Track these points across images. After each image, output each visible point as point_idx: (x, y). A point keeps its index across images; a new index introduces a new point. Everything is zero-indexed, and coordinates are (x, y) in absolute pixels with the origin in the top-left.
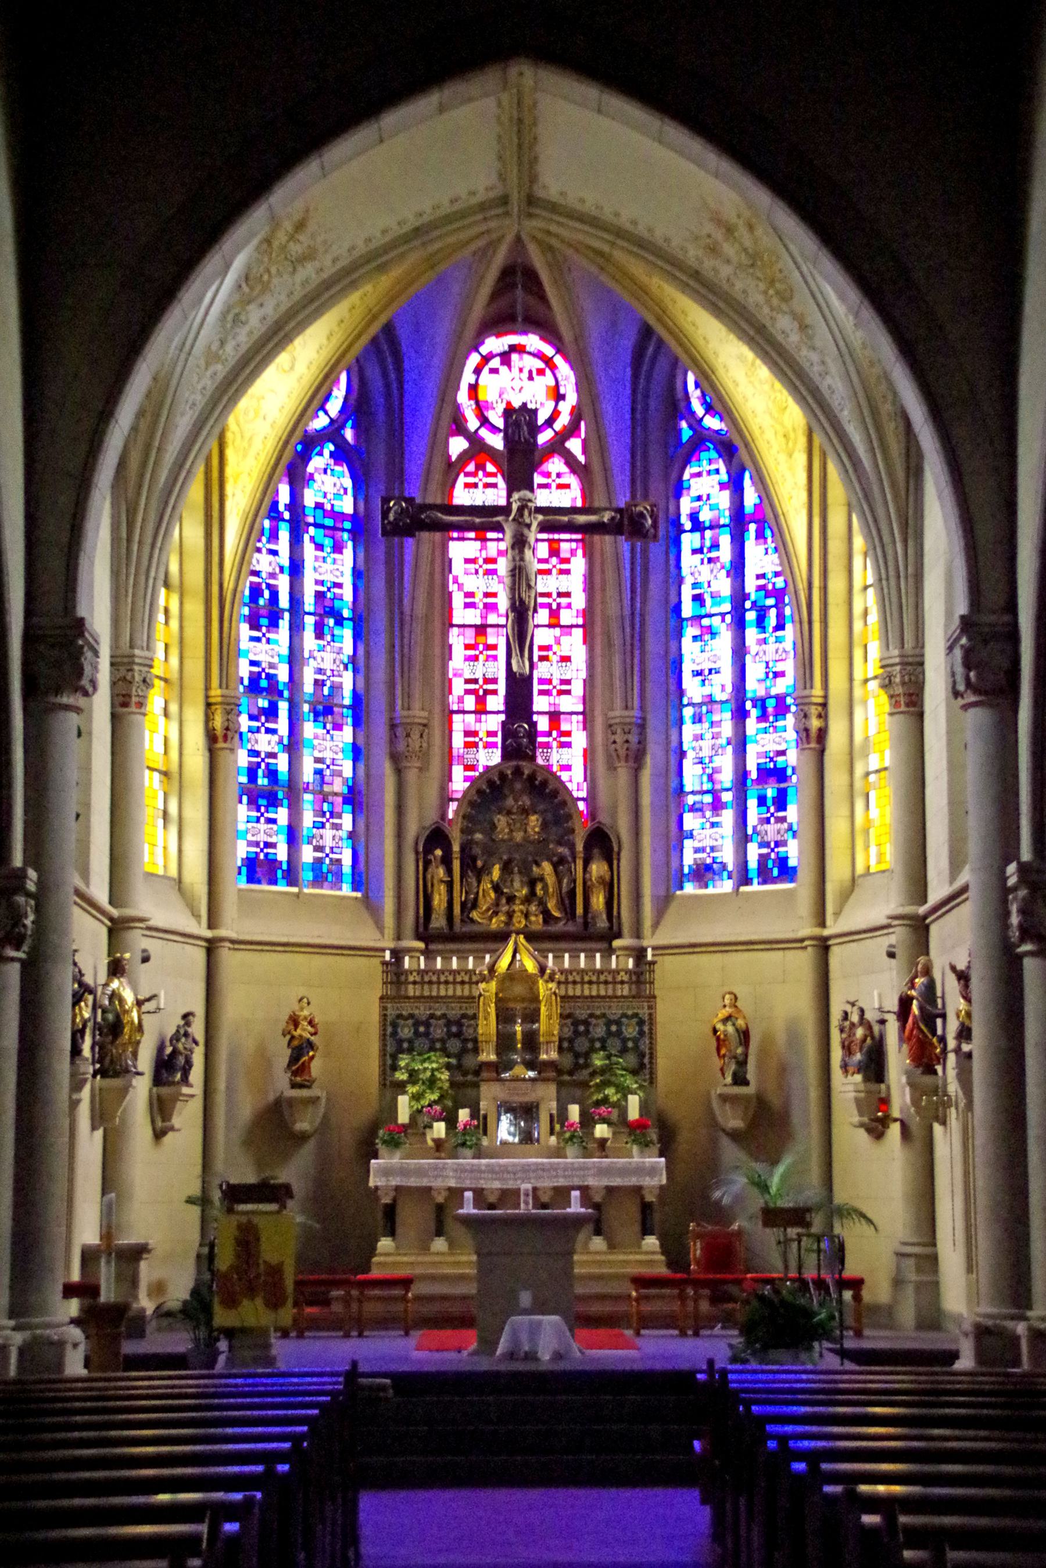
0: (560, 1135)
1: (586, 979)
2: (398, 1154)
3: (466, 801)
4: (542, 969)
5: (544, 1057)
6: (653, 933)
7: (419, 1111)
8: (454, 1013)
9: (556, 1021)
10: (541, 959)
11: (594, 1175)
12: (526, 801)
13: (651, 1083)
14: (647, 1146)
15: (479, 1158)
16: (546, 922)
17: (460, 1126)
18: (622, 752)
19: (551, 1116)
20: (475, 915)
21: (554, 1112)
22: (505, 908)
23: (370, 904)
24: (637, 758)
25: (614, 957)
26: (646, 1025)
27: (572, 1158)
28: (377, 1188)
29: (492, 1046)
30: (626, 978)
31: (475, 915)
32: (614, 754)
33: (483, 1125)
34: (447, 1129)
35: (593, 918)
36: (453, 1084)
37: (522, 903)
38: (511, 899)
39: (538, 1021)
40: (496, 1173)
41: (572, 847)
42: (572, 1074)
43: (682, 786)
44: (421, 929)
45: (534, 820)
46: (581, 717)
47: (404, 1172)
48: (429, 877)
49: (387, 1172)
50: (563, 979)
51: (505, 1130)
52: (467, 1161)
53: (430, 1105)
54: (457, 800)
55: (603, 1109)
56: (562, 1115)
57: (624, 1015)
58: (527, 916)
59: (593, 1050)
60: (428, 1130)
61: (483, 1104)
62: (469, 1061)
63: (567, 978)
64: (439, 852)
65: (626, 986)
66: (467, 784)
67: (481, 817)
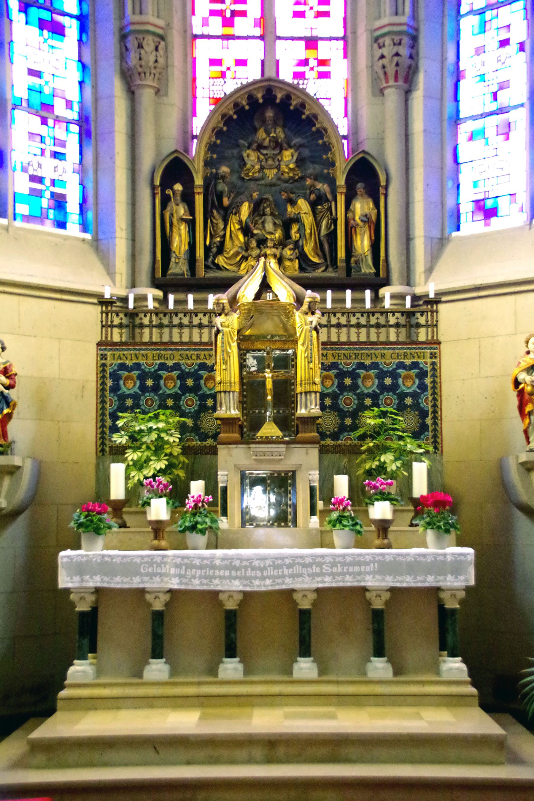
0: (324, 513)
2: (100, 541)
4: (299, 301)
5: (301, 412)
8: (189, 363)
11: (374, 573)
12: (280, 133)
13: (436, 448)
15: (216, 548)
16: (302, 269)
17: (190, 502)
18: (391, 70)
19: (312, 489)
20: (221, 260)
21: (316, 484)
23: (100, 247)
24: (407, 77)
26: (428, 379)
31: (221, 260)
33: (219, 499)
35: (356, 262)
36: (186, 451)
37: (275, 246)
40: (237, 569)
41: (332, 182)
42: (339, 435)
43: (458, 111)
44: (159, 274)
45: (288, 155)
47: (106, 567)
49: (80, 568)
51: (259, 502)
52: (199, 552)
53: (154, 476)
57: (401, 365)
59: (362, 407)
60: (147, 508)
61: (222, 476)
62: (208, 423)
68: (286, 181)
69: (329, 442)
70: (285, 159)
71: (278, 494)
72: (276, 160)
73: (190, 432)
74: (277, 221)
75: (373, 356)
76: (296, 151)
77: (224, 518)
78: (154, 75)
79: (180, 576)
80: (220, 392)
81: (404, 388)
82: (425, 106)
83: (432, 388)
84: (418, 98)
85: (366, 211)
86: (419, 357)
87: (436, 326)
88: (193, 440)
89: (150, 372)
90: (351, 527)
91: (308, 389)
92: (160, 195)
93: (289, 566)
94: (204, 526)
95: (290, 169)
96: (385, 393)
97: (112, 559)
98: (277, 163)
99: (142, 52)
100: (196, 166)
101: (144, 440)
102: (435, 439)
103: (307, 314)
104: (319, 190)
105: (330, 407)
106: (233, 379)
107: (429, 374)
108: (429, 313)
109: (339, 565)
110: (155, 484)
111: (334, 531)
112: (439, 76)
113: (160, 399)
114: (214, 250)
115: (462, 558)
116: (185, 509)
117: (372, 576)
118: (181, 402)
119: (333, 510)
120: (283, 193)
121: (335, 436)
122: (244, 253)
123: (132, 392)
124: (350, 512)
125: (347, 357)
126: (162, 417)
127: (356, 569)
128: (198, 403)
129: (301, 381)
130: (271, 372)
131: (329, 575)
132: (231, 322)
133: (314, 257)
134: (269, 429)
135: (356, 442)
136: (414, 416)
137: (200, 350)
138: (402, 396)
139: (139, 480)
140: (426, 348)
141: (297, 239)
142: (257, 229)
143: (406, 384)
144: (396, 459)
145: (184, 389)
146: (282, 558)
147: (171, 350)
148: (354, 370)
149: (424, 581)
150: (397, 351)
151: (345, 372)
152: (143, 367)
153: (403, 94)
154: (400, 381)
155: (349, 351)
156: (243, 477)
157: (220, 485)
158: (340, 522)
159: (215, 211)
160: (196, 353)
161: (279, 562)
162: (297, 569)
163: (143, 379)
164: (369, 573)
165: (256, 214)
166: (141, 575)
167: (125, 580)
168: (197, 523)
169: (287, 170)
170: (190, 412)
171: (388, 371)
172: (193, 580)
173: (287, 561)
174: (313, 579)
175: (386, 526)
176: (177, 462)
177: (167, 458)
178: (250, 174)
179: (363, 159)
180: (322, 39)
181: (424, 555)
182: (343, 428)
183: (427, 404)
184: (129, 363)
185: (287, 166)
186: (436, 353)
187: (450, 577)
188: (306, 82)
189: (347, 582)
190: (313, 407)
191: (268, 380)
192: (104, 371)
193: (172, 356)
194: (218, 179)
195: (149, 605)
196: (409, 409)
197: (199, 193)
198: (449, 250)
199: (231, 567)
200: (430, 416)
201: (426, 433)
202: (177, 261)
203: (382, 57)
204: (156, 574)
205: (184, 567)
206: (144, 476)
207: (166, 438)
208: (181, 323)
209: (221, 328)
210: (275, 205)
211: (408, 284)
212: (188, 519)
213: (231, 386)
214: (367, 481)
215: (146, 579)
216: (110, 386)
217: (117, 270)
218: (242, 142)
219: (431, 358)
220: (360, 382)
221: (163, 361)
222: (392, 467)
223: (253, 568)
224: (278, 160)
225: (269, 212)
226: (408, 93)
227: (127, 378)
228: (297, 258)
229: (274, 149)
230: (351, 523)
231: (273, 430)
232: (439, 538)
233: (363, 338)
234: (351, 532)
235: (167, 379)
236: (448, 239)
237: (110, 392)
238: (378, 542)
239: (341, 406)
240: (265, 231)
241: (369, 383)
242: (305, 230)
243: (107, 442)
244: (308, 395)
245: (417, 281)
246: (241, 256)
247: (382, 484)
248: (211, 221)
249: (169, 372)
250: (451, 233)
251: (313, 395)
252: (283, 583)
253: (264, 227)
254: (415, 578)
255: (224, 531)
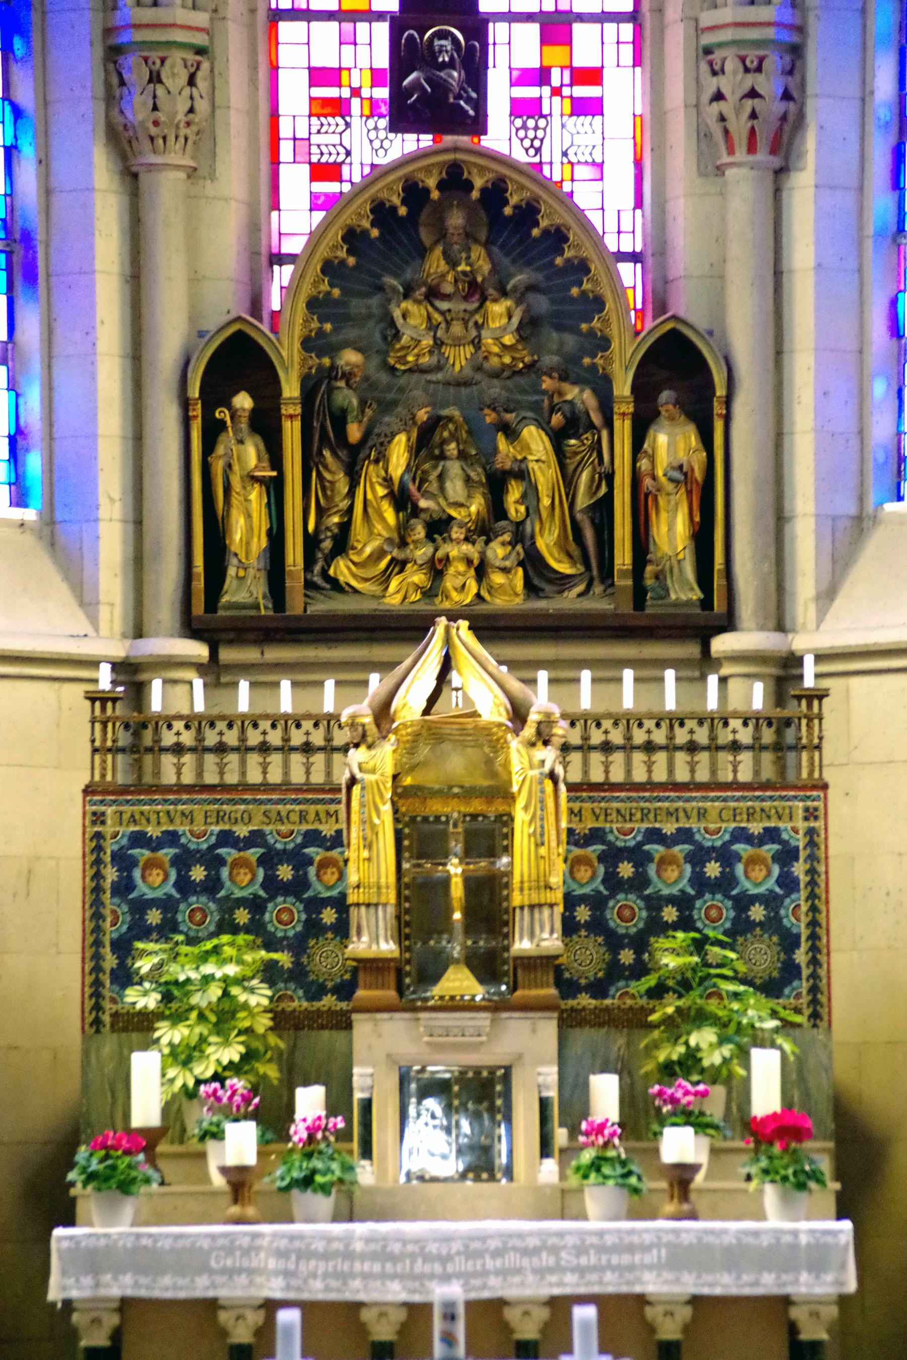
1: (639, 737)
2: (128, 1208)
3: (317, 266)
4: (518, 714)
5: (522, 945)
6: (820, 620)
7: (190, 1094)
8: (283, 833)
9: (556, 851)
10: (515, 685)
11: (657, 1267)
12: (480, 262)
13: (815, 1016)
14: (801, 1186)
15: (351, 1219)
16: (531, 589)
17: (298, 1131)
18: (740, 127)
19: (544, 1104)
20: (342, 569)
21: (552, 1094)
22: (422, 553)
23: (60, 537)
25: (713, 680)
26: (799, 863)
27: (601, 1212)
28: (68, 1304)
29: (385, 918)
30: (745, 736)
31: (342, 569)
32: (717, 130)
34: (263, 1143)
36: (282, 1021)
38: (438, 527)
39: (508, 850)
40: (394, 1258)
42: (602, 990)
44: (199, 608)
46: (627, 30)
47: (143, 1259)
48: (218, 467)
50: (575, 738)
51: (427, 1143)
52: (315, 1226)
53: (216, 1077)
54: (292, 258)
55: (682, 1088)
56: (574, 1103)
57: (741, 835)
58: (481, 571)
59: (656, 927)
60: (211, 1146)
62: (326, 960)
63: (588, 736)
64: (243, 401)
65: (746, 758)
66: (319, 215)
67: (357, 306)
68: (496, 375)
69: (585, 1001)
70: (492, 325)
71: (476, 1117)
72: (471, 324)
73: (286, 981)
74: (472, 474)
75: (681, 815)
76: (518, 302)
77: (365, 1163)
78: (186, 139)
79: (287, 1274)
80: (358, 905)
81: (747, 884)
82: (818, 210)
83: (808, 884)
84: (803, 186)
85: (682, 456)
86: (780, 818)
87: (818, 747)
88: (291, 999)
89: (198, 851)
90: (620, 1181)
91: (535, 901)
92: (200, 419)
93: (497, 1253)
94: (328, 1178)
95: (505, 347)
96: (708, 896)
97: (155, 1242)
98: (474, 333)
99: (160, 91)
100: (284, 354)
101: (195, 999)
102: (815, 995)
103: (533, 745)
104: (571, 402)
105: (588, 926)
106: (383, 880)
107: (803, 855)
108: (804, 722)
109: (592, 1252)
110: (225, 1095)
111: (586, 1190)
112: (853, 137)
113: (221, 910)
114: (327, 544)
115: (829, 1239)
116: (290, 1145)
117: (655, 1273)
118: (267, 917)
119: (585, 1146)
120: (487, 411)
121: (599, 989)
122: (395, 553)
123: (159, 894)
124: (619, 1150)
125: (624, 817)
126: (228, 951)
127: (626, 1259)
128: (304, 917)
129: (522, 882)
130: (461, 863)
131: (573, 1270)
132: (377, 763)
133: (560, 562)
134: (459, 982)
135: (643, 1002)
136: (769, 947)
137: (307, 801)
138: (743, 903)
139: (184, 1086)
140: (795, 797)
141: (521, 517)
142: (426, 495)
143: (753, 875)
144: (722, 1040)
145: (273, 886)
146: (483, 1238)
147: (244, 801)
148: (640, 845)
149: (757, 1283)
150: (732, 804)
151: (620, 850)
152: (183, 840)
153: (770, 177)
154: (740, 869)
155: (629, 805)
156: (404, 1080)
157: (358, 1095)
158: (598, 1170)
159: (327, 453)
160: (298, 808)
161: (476, 1245)
162: (512, 1259)
163: (179, 862)
164: (650, 1267)
165: (423, 453)
166: (212, 1272)
167: (181, 1282)
168: (314, 1172)
169: (496, 349)
170: (285, 938)
171: (626, 935)
172: (311, 1281)
173: (493, 1244)
174: (542, 1278)
175: (687, 1176)
176: (262, 1049)
177: (242, 1038)
178: (410, 358)
179: (673, 332)
180: (581, 18)
181: (756, 1234)
182: (615, 972)
183: (798, 920)
184: (153, 831)
185: (497, 339)
186: (816, 809)
187: (804, 1277)
188: (542, 123)
189: (608, 1284)
190: (546, 935)
191: (454, 880)
192: (99, 849)
193: (246, 816)
194: (336, 378)
195: (224, 1333)
196: (758, 931)
197: (291, 417)
198: (875, 544)
199: (384, 1256)
200: (804, 946)
201: (796, 983)
202: (241, 573)
203: (719, 96)
204: (240, 1271)
205: (293, 1257)
206: (196, 1077)
207: (243, 998)
208: (264, 743)
209: (359, 776)
210: (470, 432)
211: (781, 627)
212: (297, 1164)
213: (379, 894)
214: (657, 1087)
215: (220, 1279)
216: (113, 883)
217: (102, 597)
218: (390, 281)
219: (806, 819)
220: (652, 870)
221: (227, 827)
222: (713, 1058)
223: (427, 1258)
224: (476, 323)
225: (455, 452)
226: (781, 172)
227: (150, 865)
228: (521, 564)
229: (466, 298)
230: (619, 1170)
231: (465, 983)
232: (785, 1199)
233: (660, 775)
234: (618, 1188)
235: (236, 864)
236: (875, 519)
237: (113, 895)
238: (670, 1208)
239: (612, 924)
240: (446, 498)
241: (671, 874)
242: (538, 500)
243: (107, 1005)
244: (536, 911)
245: (800, 620)
246: (389, 558)
247: (687, 1093)
248: (320, 476)
249: (240, 850)
250: (881, 504)
251: (546, 912)
252: (484, 1287)
253: (442, 489)
254: (739, 1277)
255: (369, 1191)
